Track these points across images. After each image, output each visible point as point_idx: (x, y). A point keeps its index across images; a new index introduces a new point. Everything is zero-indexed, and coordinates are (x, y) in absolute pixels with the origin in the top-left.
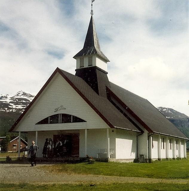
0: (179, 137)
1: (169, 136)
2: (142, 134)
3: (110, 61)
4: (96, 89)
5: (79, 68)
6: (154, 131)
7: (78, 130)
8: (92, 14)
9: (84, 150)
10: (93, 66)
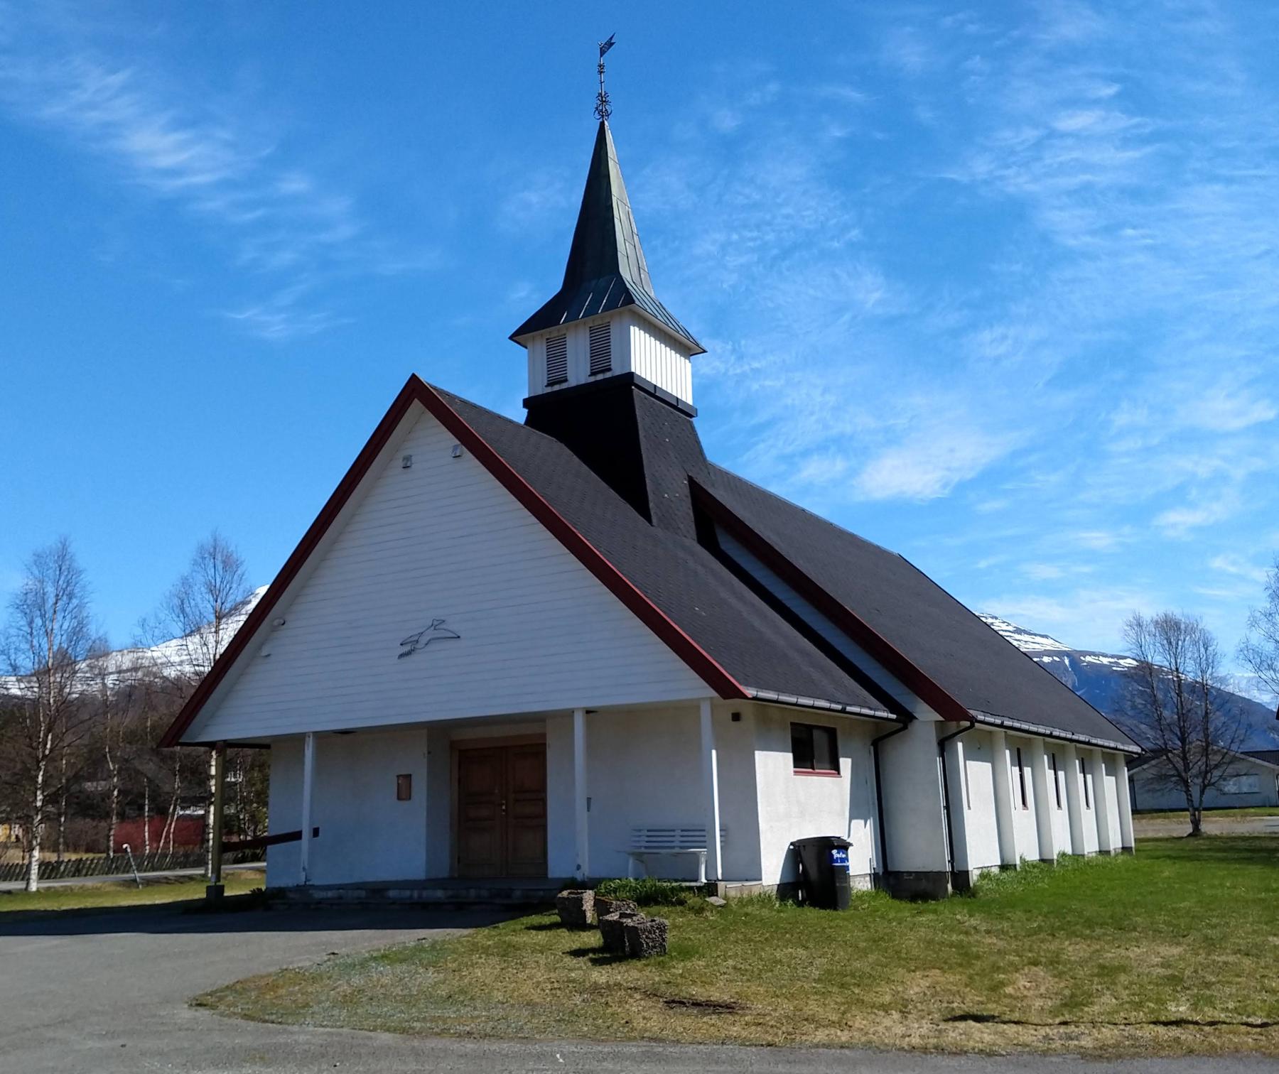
0: (1094, 741)
1: (1051, 736)
2: (905, 728)
3: (705, 351)
4: (629, 482)
5: (541, 389)
6: (972, 712)
7: (539, 718)
8: (603, 114)
9: (578, 838)
10: (617, 370)
